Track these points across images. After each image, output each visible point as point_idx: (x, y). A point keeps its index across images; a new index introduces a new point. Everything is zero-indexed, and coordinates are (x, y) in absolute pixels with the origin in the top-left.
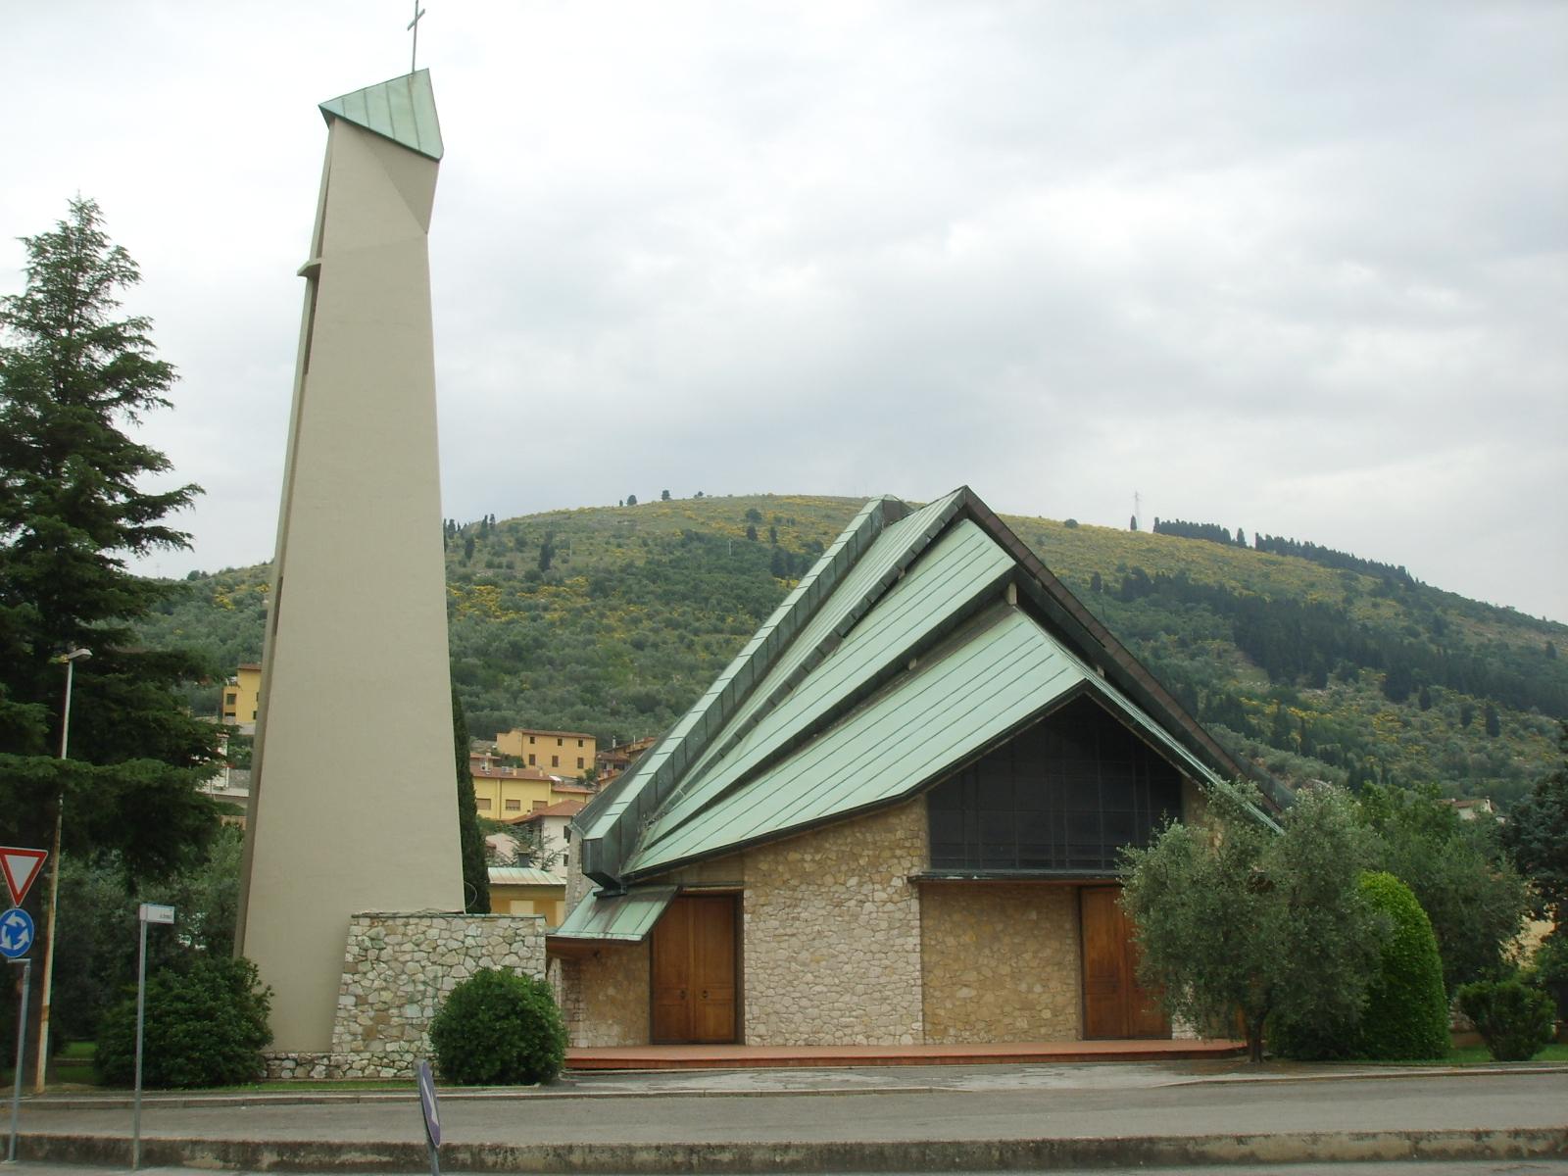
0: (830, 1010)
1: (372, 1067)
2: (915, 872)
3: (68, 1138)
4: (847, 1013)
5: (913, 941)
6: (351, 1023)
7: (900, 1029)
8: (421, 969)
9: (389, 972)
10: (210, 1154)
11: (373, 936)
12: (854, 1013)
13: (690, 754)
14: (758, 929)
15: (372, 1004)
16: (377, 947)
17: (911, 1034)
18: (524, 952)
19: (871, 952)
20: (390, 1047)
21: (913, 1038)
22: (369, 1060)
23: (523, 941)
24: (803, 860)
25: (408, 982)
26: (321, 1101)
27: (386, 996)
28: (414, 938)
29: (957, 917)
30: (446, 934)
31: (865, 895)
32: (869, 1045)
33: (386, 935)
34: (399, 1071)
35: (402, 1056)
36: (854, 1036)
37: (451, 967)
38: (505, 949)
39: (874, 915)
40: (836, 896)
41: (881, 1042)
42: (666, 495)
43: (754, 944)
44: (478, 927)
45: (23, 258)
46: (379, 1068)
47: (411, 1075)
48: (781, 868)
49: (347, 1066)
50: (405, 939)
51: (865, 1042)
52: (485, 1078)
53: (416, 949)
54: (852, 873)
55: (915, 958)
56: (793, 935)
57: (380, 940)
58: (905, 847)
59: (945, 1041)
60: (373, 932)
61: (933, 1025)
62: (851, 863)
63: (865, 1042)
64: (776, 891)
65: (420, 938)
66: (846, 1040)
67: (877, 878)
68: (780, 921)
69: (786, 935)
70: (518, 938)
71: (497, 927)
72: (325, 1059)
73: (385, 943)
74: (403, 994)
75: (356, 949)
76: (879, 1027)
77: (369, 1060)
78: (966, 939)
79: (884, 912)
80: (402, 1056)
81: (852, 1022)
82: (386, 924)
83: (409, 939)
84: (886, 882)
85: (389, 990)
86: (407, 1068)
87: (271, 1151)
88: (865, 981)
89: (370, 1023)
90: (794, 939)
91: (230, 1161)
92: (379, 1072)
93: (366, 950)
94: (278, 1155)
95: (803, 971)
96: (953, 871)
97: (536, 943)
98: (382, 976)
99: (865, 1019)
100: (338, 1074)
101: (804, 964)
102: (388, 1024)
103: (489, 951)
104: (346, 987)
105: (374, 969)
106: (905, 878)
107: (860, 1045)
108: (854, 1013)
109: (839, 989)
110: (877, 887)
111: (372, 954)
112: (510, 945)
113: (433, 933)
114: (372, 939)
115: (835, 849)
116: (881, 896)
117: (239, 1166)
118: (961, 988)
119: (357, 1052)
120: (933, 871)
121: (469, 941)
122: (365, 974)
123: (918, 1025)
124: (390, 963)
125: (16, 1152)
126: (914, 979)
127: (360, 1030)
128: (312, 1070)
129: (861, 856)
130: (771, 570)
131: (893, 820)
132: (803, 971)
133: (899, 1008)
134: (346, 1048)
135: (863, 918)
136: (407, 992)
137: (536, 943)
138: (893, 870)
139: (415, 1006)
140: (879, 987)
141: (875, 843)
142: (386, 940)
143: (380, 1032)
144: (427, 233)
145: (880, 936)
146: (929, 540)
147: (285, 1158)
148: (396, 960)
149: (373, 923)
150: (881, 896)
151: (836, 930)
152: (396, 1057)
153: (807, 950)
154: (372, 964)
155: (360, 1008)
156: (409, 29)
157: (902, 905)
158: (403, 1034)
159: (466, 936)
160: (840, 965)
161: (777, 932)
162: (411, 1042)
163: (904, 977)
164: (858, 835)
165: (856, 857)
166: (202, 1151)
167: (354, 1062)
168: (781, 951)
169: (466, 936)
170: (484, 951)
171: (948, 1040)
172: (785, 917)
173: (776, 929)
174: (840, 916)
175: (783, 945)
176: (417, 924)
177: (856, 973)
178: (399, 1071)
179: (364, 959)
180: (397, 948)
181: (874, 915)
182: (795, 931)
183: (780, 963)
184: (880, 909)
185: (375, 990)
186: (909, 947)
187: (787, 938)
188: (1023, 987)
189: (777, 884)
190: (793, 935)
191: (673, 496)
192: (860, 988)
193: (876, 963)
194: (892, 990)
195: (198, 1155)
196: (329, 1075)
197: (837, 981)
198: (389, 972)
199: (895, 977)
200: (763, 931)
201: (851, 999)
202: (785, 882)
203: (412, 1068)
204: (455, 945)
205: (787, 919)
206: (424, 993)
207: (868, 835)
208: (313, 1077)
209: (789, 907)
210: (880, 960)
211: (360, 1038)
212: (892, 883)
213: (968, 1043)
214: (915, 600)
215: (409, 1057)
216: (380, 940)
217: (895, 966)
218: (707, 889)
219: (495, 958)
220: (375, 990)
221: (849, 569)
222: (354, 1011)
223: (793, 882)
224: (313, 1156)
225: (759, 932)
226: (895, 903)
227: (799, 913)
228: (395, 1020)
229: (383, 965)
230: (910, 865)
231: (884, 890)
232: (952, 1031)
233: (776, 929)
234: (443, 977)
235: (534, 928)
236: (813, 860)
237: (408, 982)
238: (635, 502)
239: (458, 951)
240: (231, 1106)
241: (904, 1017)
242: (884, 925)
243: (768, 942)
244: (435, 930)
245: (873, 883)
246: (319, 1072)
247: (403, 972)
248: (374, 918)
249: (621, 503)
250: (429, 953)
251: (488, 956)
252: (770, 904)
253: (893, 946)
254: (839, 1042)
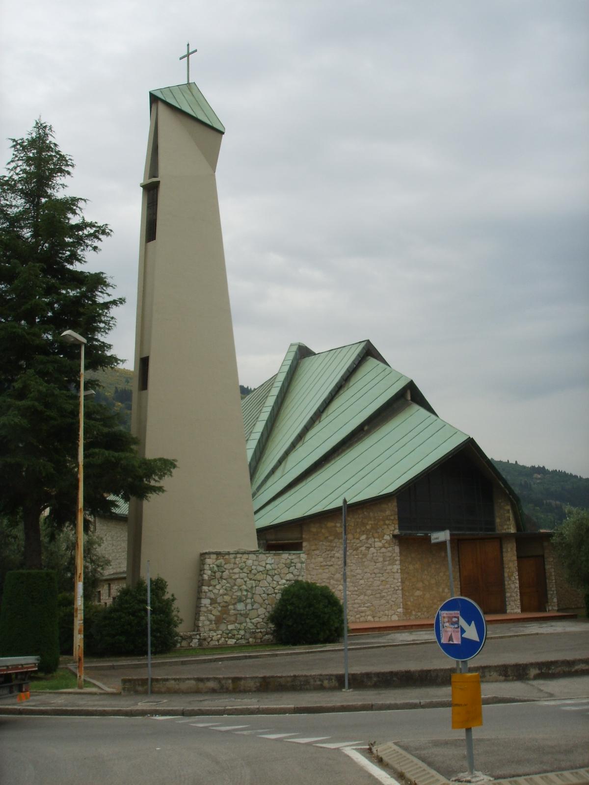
0: (353, 604)
1: (223, 639)
2: (397, 532)
3: (391, 673)
4: (362, 605)
5: (397, 567)
6: (209, 615)
7: (391, 612)
8: (244, 583)
9: (228, 585)
10: (495, 674)
11: (218, 565)
12: (366, 605)
14: (311, 563)
15: (219, 603)
16: (221, 571)
17: (397, 615)
18: (296, 572)
19: (374, 573)
20: (230, 627)
21: (398, 617)
22: (221, 635)
23: (295, 566)
24: (335, 526)
25: (238, 590)
26: (256, 657)
27: (227, 598)
28: (240, 565)
29: (413, 555)
30: (256, 563)
31: (370, 544)
32: (374, 621)
33: (225, 564)
34: (237, 640)
35: (238, 632)
36: (366, 617)
37: (259, 581)
38: (286, 570)
39: (375, 554)
40: (355, 544)
41: (382, 620)
43: (309, 571)
44: (272, 559)
45: (10, 153)
46: (227, 639)
47: (244, 642)
48: (323, 531)
49: (210, 639)
50: (235, 566)
51: (372, 619)
52: (322, 639)
53: (241, 571)
54: (363, 533)
55: (398, 576)
56: (331, 565)
57: (222, 567)
59: (411, 618)
60: (218, 562)
61: (407, 611)
62: (362, 528)
63: (372, 619)
64: (321, 543)
65: (243, 565)
66: (362, 619)
67: (376, 535)
68: (324, 558)
69: (327, 565)
70: (292, 565)
71: (282, 558)
72: (198, 636)
73: (225, 569)
74: (236, 597)
75: (209, 572)
76: (379, 611)
77: (221, 635)
78: (417, 566)
79: (381, 553)
80: (238, 632)
81: (365, 610)
82: (225, 557)
83: (237, 566)
84: (381, 537)
85: (228, 595)
86: (241, 638)
87: (534, 668)
88: (371, 588)
89: (218, 614)
90: (331, 568)
91: (509, 676)
92: (227, 641)
93: (215, 573)
94: (539, 669)
95: (337, 584)
96: (420, 532)
97: (302, 567)
98: (224, 587)
99: (372, 607)
100: (205, 643)
101: (337, 580)
102: (228, 614)
103: (278, 571)
104: (205, 594)
105: (219, 583)
106: (391, 535)
107: (370, 621)
108: (366, 605)
109: (357, 593)
110: (376, 540)
111: (218, 575)
112: (289, 568)
113: (249, 562)
114: (218, 566)
115: (353, 520)
116: (378, 544)
117: (515, 678)
118: (416, 591)
119: (215, 631)
120: (404, 532)
121: (268, 567)
122: (215, 586)
123: (400, 610)
124: (228, 580)
125: (349, 684)
126: (398, 587)
127: (213, 618)
128: (191, 642)
129: (367, 524)
131: (384, 506)
132: (337, 584)
133: (390, 601)
134: (207, 628)
135: (369, 556)
136: (237, 596)
137: (302, 567)
138: (385, 531)
139: (242, 603)
140: (379, 591)
142: (225, 566)
143: (224, 619)
144: (215, 172)
145: (379, 565)
146: (355, 366)
147: (543, 671)
148: (231, 578)
149: (218, 557)
150: (378, 544)
151: (355, 562)
152: (236, 632)
153: (339, 573)
154: (219, 580)
155: (213, 605)
156: (181, 59)
157: (390, 549)
158: (236, 619)
159: (267, 564)
160: (358, 581)
161: (322, 564)
162: (241, 624)
163: (392, 586)
164: (365, 513)
165: (364, 525)
166: (490, 672)
167: (213, 636)
168: (324, 574)
169: (267, 564)
170: (276, 572)
171: (412, 617)
172: (326, 556)
173: (321, 562)
174: (356, 555)
175: (327, 571)
176: (241, 557)
177: (367, 584)
178: (237, 640)
179: (214, 577)
180: (231, 571)
181: (375, 554)
182: (332, 563)
183: (324, 580)
185: (221, 595)
186: (395, 570)
187: (327, 567)
188: (441, 590)
190: (331, 565)
192: (369, 592)
193: (378, 579)
194: (386, 593)
195: (487, 674)
196: (200, 644)
197: (356, 589)
198: (228, 585)
199: (388, 586)
200: (314, 564)
201: (364, 598)
202: (326, 538)
203: (244, 639)
204: (261, 569)
205: (327, 557)
206: (246, 596)
207: (371, 513)
208: (191, 646)
209: (328, 551)
210: (379, 577)
211: (213, 622)
212: (385, 538)
213: (420, 618)
214: (358, 395)
215: (242, 632)
216: (222, 567)
217: (387, 580)
218: (282, 542)
219: (282, 575)
220: (221, 595)
222: (210, 608)
223: (330, 538)
224: (560, 668)
225: (312, 564)
226: (386, 548)
227: (334, 554)
228: (232, 612)
229: (224, 581)
230: (393, 529)
231: (380, 541)
232: (414, 613)
233: (321, 562)
234: (256, 587)
235: (300, 559)
237: (238, 590)
239: (263, 572)
240: (208, 662)
241: (393, 606)
242: (381, 559)
243: (317, 569)
244: (250, 561)
245: (374, 538)
246: (195, 643)
247: (235, 585)
248: (218, 554)
250: (248, 573)
251: (278, 574)
252: (318, 549)
253: (386, 570)
254: (358, 620)
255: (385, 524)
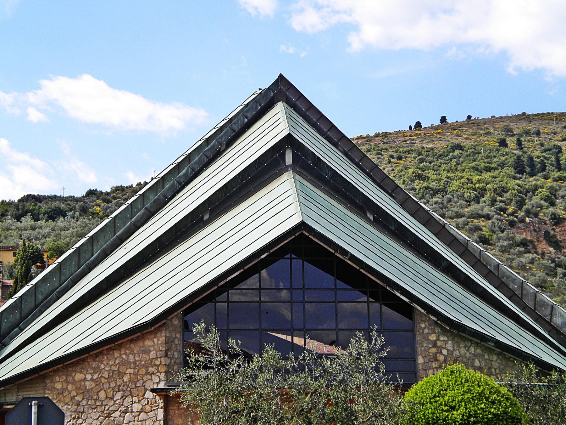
13: (40, 297)
42: (443, 119)
58: (155, 365)
129: (125, 374)
130: (515, 169)
141: (135, 363)
150: (136, 407)
184: (136, 418)
189: (67, 400)
191: (449, 120)
209: (74, 418)
221: (230, 143)
236: (92, 380)
238: (421, 126)
249: (410, 127)
255: (147, 373)
